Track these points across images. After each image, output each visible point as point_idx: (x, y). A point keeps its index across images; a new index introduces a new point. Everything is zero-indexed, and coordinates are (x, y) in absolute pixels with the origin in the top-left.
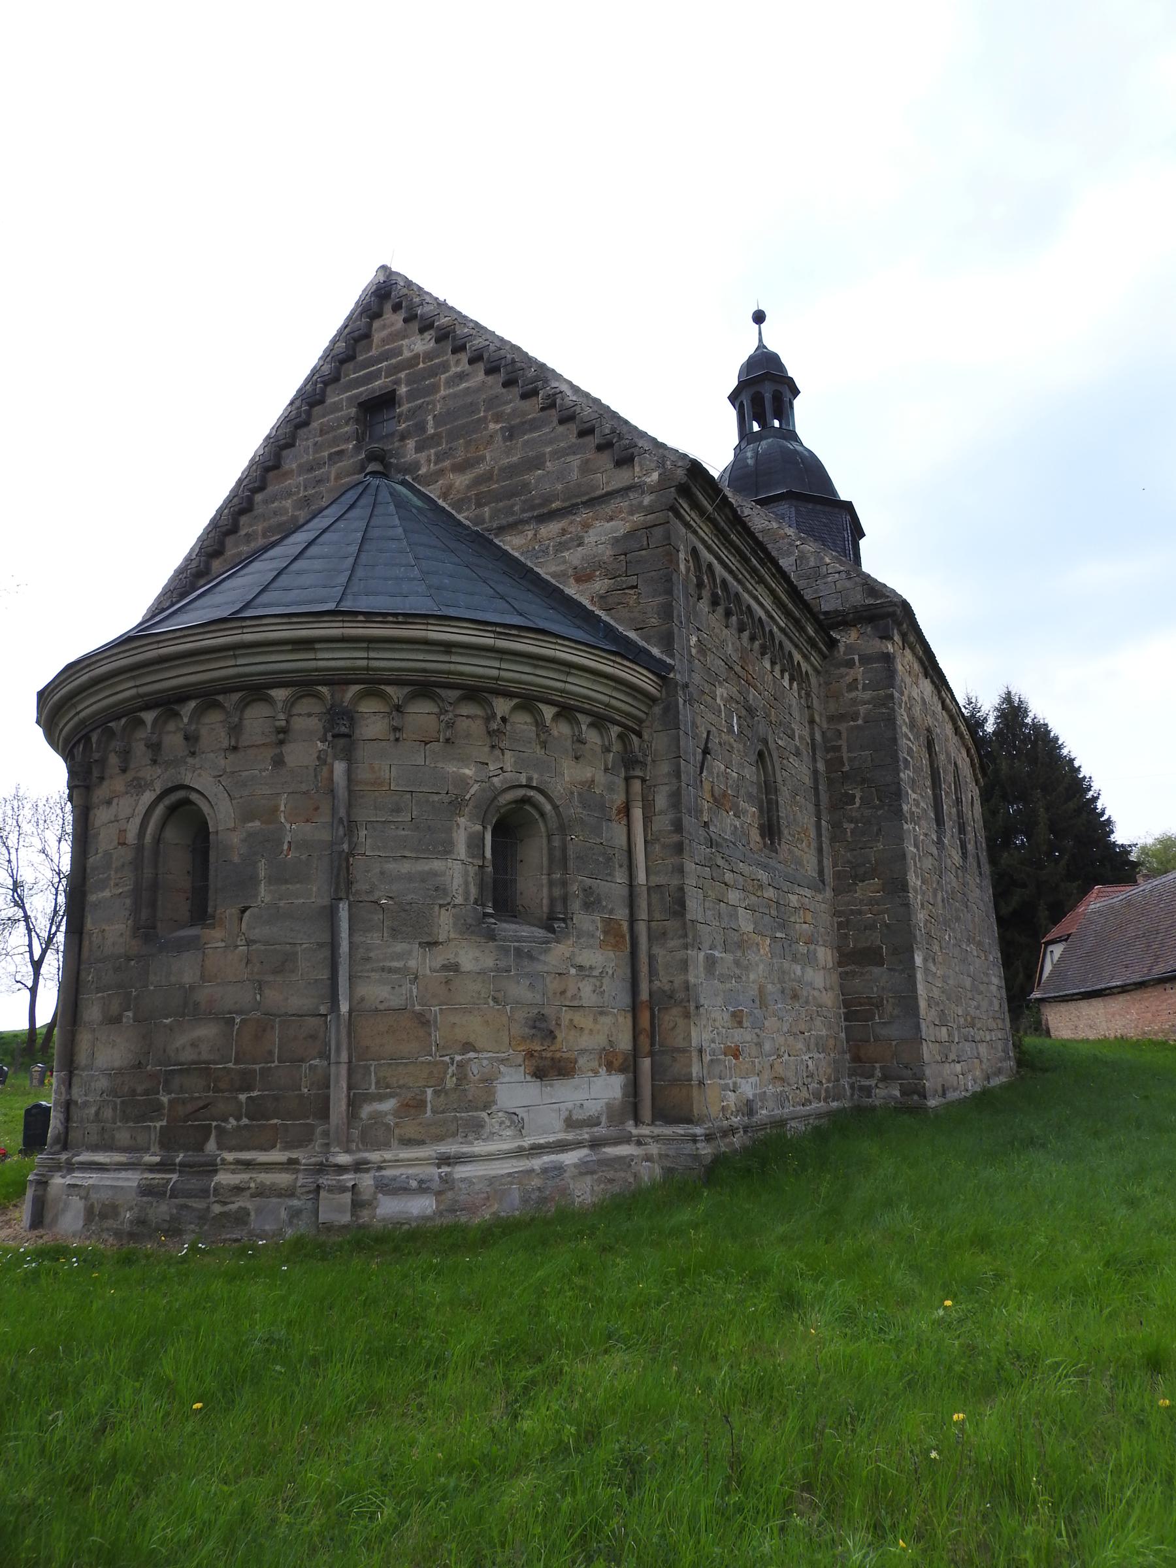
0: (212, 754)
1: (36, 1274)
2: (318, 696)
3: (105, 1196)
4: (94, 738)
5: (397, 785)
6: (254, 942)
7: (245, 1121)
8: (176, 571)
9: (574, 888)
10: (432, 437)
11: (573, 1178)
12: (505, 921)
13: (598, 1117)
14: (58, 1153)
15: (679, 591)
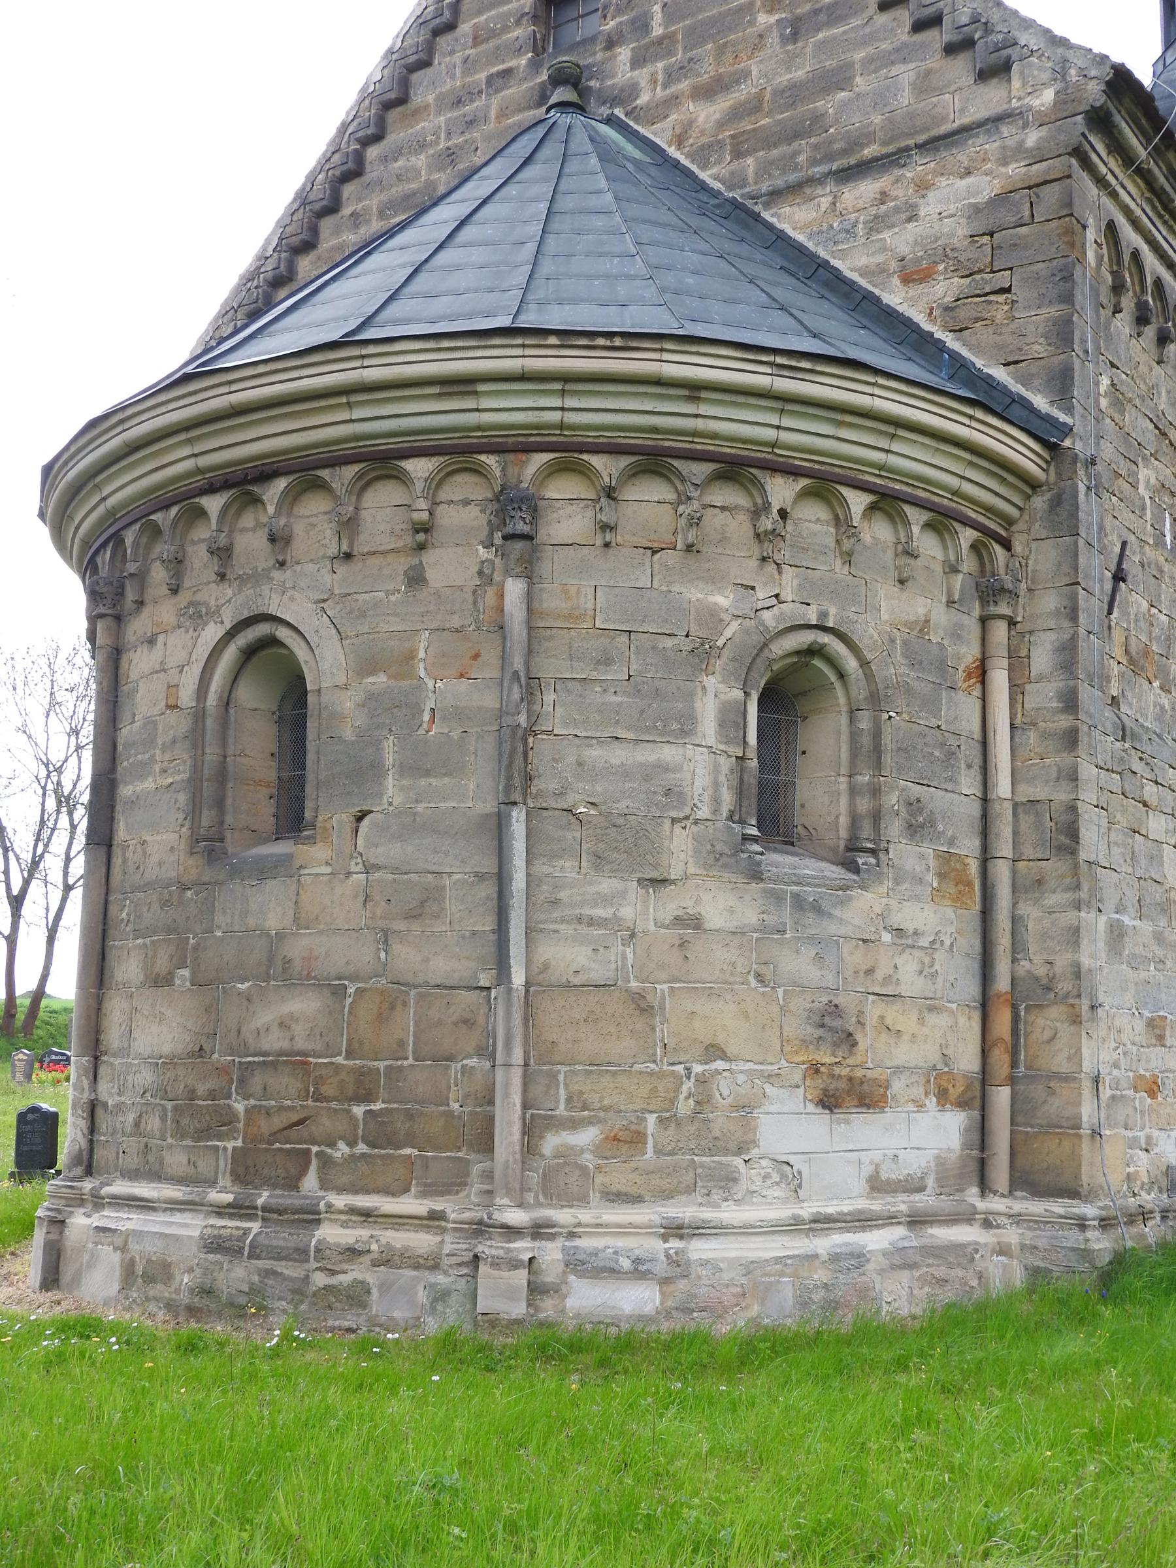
1: (60, 1357)
2: (478, 471)
3: (152, 1248)
4: (129, 537)
6: (377, 867)
7: (362, 1148)
8: (242, 277)
9: (892, 799)
10: (660, 41)
11: (881, 1272)
12: (775, 850)
13: (922, 1178)
14: (80, 1179)
15: (1084, 299)
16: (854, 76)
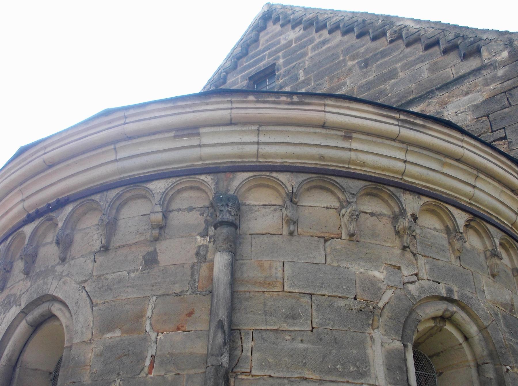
0: (81, 259)
5: (291, 286)
10: (303, 82)
16: (398, 73)
